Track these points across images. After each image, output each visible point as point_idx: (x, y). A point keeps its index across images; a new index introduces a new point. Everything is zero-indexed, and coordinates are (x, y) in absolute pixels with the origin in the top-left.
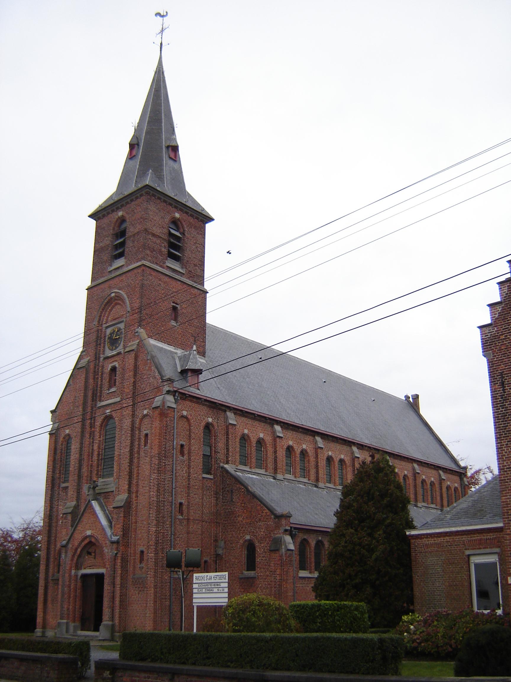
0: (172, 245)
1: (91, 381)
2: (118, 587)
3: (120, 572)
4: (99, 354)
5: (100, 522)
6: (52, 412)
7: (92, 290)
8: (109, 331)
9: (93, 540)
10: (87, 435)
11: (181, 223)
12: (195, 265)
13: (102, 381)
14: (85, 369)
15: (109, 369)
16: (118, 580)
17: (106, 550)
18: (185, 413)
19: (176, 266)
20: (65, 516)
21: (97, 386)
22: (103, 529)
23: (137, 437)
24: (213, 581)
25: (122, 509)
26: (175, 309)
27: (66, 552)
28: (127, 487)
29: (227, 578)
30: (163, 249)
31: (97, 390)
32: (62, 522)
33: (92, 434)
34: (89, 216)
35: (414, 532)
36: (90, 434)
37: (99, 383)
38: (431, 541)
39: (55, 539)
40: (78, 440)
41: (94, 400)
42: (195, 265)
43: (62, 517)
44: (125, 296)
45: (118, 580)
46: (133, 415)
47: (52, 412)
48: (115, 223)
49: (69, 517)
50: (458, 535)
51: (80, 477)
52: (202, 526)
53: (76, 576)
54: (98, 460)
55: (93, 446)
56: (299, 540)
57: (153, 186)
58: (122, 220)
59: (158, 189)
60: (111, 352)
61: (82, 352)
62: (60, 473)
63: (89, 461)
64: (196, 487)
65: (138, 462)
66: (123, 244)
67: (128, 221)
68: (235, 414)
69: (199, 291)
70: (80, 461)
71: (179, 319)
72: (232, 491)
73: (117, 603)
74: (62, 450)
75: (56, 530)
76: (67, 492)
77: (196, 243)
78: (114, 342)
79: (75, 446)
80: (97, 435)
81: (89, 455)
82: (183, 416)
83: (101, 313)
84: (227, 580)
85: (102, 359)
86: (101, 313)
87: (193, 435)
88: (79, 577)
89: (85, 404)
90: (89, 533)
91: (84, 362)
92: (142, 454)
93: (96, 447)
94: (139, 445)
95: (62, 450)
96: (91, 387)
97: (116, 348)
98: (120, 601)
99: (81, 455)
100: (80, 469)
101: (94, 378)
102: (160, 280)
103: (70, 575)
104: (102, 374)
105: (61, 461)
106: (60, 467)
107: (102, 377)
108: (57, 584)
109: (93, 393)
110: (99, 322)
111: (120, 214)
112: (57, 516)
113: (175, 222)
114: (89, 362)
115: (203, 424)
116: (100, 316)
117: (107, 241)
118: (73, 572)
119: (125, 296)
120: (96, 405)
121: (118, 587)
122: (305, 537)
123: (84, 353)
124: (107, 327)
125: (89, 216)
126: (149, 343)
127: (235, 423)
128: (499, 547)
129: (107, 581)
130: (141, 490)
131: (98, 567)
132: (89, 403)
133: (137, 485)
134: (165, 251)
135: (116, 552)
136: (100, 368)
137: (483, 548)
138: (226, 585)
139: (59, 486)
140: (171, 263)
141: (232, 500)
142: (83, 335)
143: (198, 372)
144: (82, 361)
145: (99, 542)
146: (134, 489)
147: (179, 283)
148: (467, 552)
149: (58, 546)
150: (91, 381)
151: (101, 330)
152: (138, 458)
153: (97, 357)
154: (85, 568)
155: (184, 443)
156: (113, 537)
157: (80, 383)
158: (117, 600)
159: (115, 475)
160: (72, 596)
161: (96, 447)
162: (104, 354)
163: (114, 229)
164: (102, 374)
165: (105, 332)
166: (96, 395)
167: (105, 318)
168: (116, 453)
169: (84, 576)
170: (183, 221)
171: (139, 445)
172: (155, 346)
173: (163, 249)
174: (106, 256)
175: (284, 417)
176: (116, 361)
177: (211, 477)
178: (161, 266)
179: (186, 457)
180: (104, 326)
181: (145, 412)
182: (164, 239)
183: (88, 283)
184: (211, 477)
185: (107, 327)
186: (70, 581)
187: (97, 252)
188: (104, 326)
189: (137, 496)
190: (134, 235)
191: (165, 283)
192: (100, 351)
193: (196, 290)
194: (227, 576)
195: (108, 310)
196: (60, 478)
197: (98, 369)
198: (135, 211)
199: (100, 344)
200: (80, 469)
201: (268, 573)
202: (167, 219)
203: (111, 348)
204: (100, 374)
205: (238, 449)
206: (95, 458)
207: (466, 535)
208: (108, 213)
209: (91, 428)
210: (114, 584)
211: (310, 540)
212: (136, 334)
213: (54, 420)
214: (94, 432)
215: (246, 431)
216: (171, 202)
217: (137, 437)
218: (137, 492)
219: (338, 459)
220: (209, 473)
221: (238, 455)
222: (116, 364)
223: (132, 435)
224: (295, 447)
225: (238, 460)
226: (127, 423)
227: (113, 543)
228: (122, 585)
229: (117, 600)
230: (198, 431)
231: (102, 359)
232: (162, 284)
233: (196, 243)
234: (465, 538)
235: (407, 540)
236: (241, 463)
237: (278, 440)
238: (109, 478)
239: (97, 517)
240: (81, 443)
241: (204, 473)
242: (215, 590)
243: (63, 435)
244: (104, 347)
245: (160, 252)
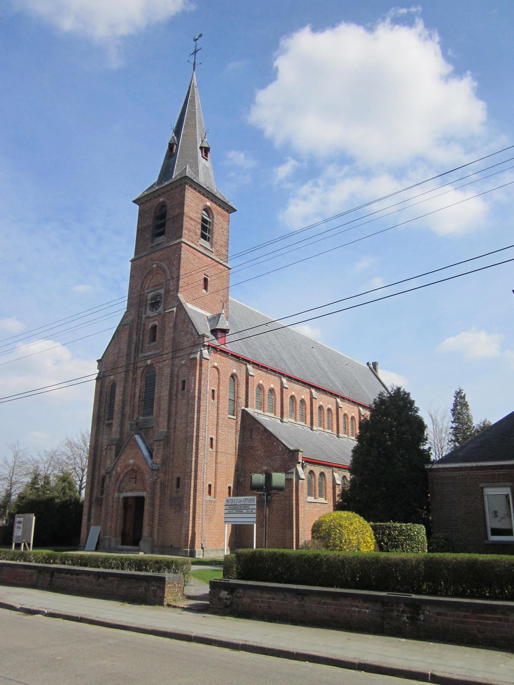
0: (204, 228)
1: (134, 336)
2: (157, 508)
3: (159, 495)
4: (141, 314)
5: (142, 452)
6: (99, 361)
7: (135, 262)
8: (150, 296)
9: (135, 468)
10: (130, 380)
11: (211, 211)
12: (222, 246)
13: (143, 337)
14: (129, 326)
15: (150, 327)
16: (157, 501)
17: (147, 476)
18: (216, 364)
19: (207, 244)
20: (109, 447)
21: (139, 340)
22: (145, 459)
23: (175, 383)
24: (242, 503)
25: (162, 442)
26: (206, 280)
27: (110, 478)
28: (166, 424)
29: (255, 501)
30: (197, 230)
31: (139, 344)
32: (106, 453)
33: (134, 380)
34: (134, 202)
35: (429, 466)
36: (133, 380)
37: (141, 338)
38: (448, 474)
39: (99, 467)
40: (122, 384)
41: (136, 351)
42: (222, 246)
43: (107, 448)
44: (166, 267)
45: (157, 501)
46: (173, 365)
47: (99, 361)
48: (156, 209)
49: (114, 447)
50: (472, 470)
51: (123, 415)
52: (227, 458)
53: (119, 498)
54: (139, 401)
55: (135, 389)
56: (308, 471)
57: (191, 177)
58: (163, 205)
59: (194, 180)
60: (152, 312)
61: (126, 313)
62: (105, 411)
63: (131, 401)
64: (223, 426)
65: (176, 404)
66: (163, 225)
67: (168, 205)
68: (253, 367)
69: (224, 268)
70: (124, 402)
71: (209, 288)
72: (251, 430)
73: (156, 522)
74: (107, 392)
75: (101, 459)
76: (111, 429)
77: (222, 228)
78: (155, 305)
79: (119, 391)
80: (139, 381)
81: (131, 397)
82: (214, 367)
83: (144, 281)
84: (255, 503)
85: (143, 318)
86: (144, 281)
87: (221, 383)
88: (121, 499)
89: (128, 355)
90: (131, 461)
91: (130, 318)
92: (180, 396)
93: (137, 390)
94: (177, 389)
95: (107, 392)
96: (134, 341)
97: (156, 309)
98: (159, 520)
99: (124, 397)
100: (123, 409)
101: (137, 335)
102: (195, 255)
103: (113, 498)
104: (144, 331)
105: (106, 402)
106: (105, 407)
107: (143, 333)
108: (101, 505)
109: (136, 347)
110: (141, 288)
111: (161, 200)
112: (102, 448)
113: (207, 209)
114: (132, 321)
115: (230, 374)
116: (143, 283)
117: (150, 222)
118: (116, 495)
119: (166, 267)
120: (138, 356)
121: (157, 508)
122: (312, 469)
123: (128, 313)
124: (148, 293)
125: (134, 202)
126: (187, 306)
127: (253, 375)
128: (512, 481)
129: (147, 502)
130: (178, 425)
131: (139, 490)
132: (133, 353)
133: (175, 423)
134: (199, 232)
135: (156, 478)
136: (142, 326)
137: (497, 482)
138: (255, 507)
139: (104, 423)
140: (202, 242)
141: (251, 437)
142: (127, 298)
143: (225, 331)
144: (126, 320)
145: (140, 470)
146: (172, 425)
147: (209, 259)
148: (481, 485)
149: (103, 472)
150: (134, 336)
151: (143, 294)
152: (176, 400)
153: (139, 317)
154: (126, 492)
155: (214, 389)
156: (153, 465)
157: (124, 338)
158: (156, 519)
159: (154, 414)
160: (114, 515)
161: (137, 390)
162: (145, 314)
163: (155, 212)
164: (144, 331)
165: (147, 296)
166: (139, 347)
167: (147, 285)
168: (156, 396)
169: (126, 499)
170: (212, 209)
171: (177, 389)
172: (191, 309)
173: (197, 230)
174: (148, 235)
175: (288, 373)
176: (156, 320)
177: (235, 417)
178: (195, 244)
179: (216, 400)
180: (146, 291)
181: (183, 362)
182: (198, 222)
183: (133, 256)
184: (235, 417)
185: (148, 293)
186: (113, 502)
187: (140, 231)
188: (146, 291)
189: (175, 432)
190: (174, 217)
191: (198, 258)
192: (142, 312)
193: (222, 266)
194: (255, 499)
195: (150, 278)
196: (104, 416)
197: (140, 327)
198: (175, 198)
199: (142, 306)
200: (123, 409)
201: (282, 498)
202: (201, 207)
203: (152, 309)
204: (142, 330)
205: (255, 396)
206: (137, 399)
207: (480, 470)
208: (150, 200)
209: (133, 375)
210: (153, 505)
211: (315, 472)
212: (176, 298)
213: (99, 368)
214: (136, 378)
215: (261, 382)
216: (205, 193)
217: (175, 383)
218: (175, 428)
219: (327, 408)
220: (234, 415)
221: (255, 400)
222: (156, 323)
223: (172, 381)
224: (296, 396)
225: (255, 405)
226: (167, 371)
227: (153, 470)
228: (161, 506)
229: (156, 519)
230: (226, 379)
231: (143, 318)
232: (196, 259)
233: (222, 228)
234: (479, 472)
235: (425, 472)
236: (257, 408)
237: (284, 389)
238: (148, 416)
239: (140, 448)
240: (125, 388)
241: (230, 414)
242: (245, 511)
243: (108, 381)
244: (146, 308)
245: (195, 232)
